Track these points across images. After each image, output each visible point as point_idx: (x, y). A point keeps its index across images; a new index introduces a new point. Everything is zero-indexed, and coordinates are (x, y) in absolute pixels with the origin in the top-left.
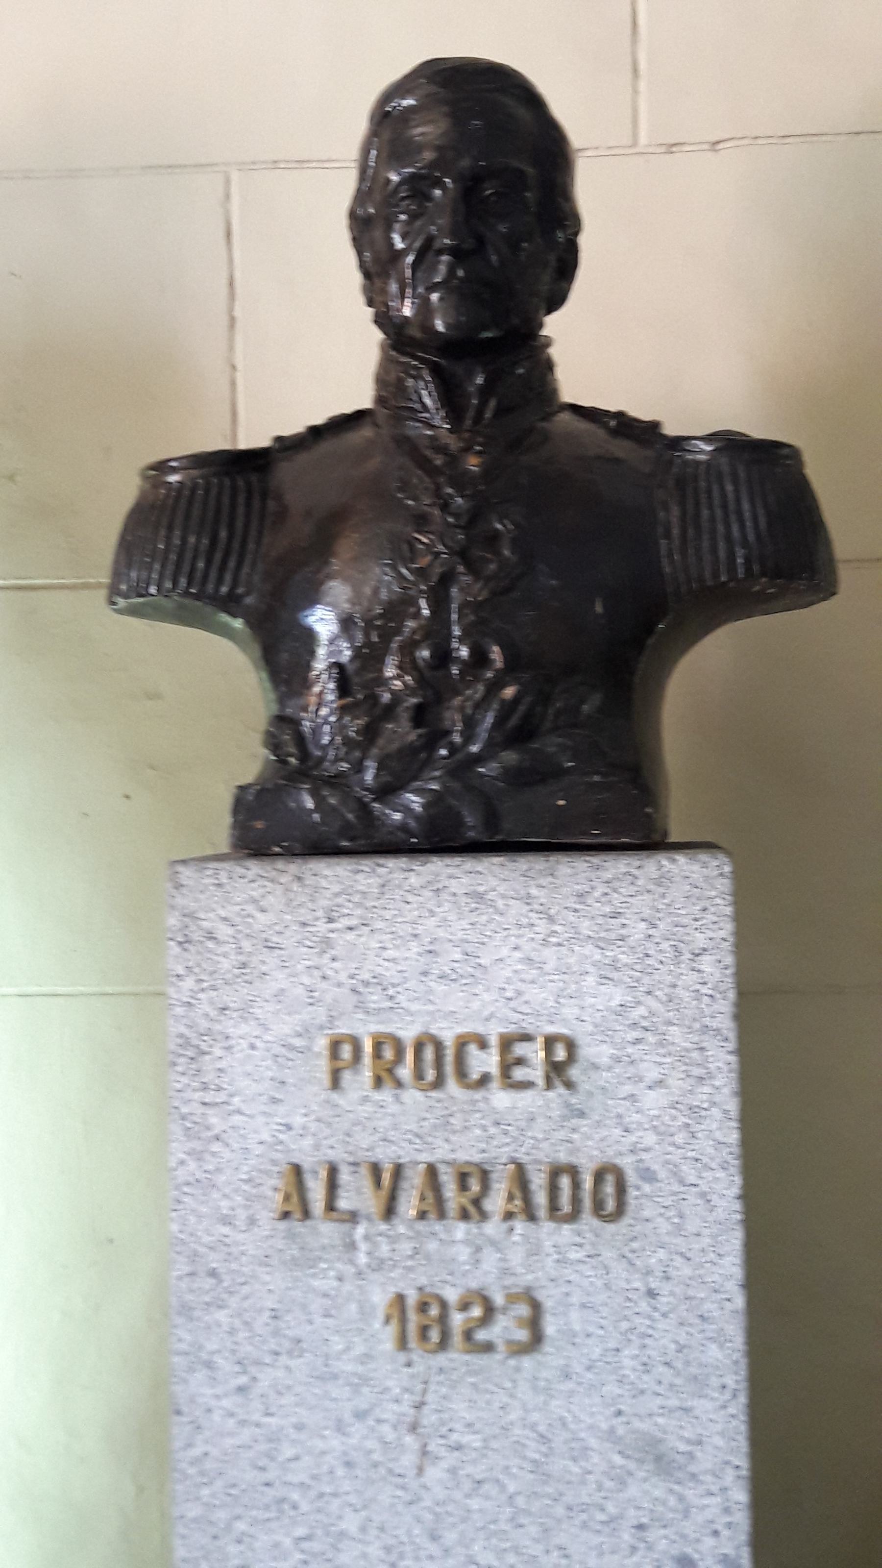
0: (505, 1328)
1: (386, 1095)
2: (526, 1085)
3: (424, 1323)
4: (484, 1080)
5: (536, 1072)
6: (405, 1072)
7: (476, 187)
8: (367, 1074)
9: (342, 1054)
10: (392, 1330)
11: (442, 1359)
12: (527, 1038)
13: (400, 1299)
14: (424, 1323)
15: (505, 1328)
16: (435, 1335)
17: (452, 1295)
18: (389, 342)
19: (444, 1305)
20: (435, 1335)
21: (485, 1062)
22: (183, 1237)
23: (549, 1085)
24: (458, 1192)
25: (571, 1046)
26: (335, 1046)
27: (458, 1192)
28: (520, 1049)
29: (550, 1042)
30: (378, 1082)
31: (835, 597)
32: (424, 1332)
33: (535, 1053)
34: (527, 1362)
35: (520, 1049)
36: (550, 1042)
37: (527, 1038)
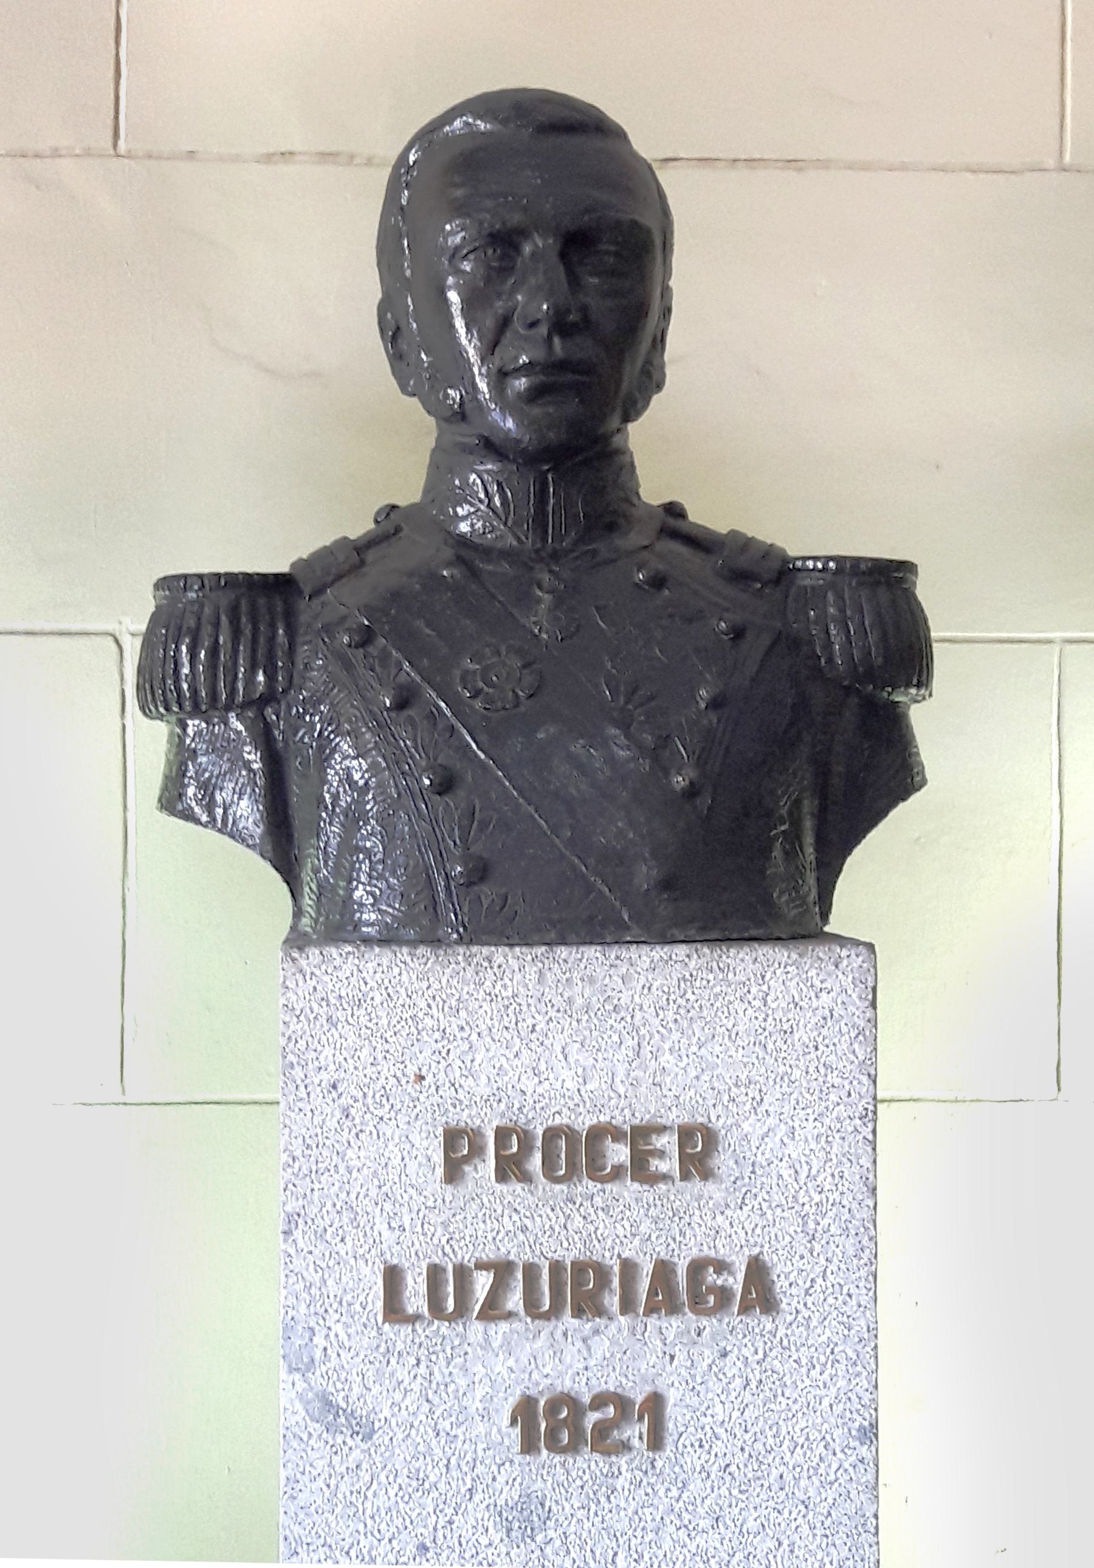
1: (282, 1237)
2: (665, 1177)
3: (551, 1424)
4: (617, 1173)
5: (669, 1165)
6: (536, 1162)
7: (544, 241)
8: (489, 1164)
9: (458, 1149)
12: (662, 1129)
14: (551, 1424)
16: (565, 1437)
18: (915, 750)
20: (565, 1437)
21: (619, 1153)
23: (685, 1176)
24: (579, 1289)
25: (710, 1137)
27: (579, 1289)
29: (686, 1134)
30: (502, 1176)
33: (668, 1142)
36: (686, 1134)
37: (662, 1129)
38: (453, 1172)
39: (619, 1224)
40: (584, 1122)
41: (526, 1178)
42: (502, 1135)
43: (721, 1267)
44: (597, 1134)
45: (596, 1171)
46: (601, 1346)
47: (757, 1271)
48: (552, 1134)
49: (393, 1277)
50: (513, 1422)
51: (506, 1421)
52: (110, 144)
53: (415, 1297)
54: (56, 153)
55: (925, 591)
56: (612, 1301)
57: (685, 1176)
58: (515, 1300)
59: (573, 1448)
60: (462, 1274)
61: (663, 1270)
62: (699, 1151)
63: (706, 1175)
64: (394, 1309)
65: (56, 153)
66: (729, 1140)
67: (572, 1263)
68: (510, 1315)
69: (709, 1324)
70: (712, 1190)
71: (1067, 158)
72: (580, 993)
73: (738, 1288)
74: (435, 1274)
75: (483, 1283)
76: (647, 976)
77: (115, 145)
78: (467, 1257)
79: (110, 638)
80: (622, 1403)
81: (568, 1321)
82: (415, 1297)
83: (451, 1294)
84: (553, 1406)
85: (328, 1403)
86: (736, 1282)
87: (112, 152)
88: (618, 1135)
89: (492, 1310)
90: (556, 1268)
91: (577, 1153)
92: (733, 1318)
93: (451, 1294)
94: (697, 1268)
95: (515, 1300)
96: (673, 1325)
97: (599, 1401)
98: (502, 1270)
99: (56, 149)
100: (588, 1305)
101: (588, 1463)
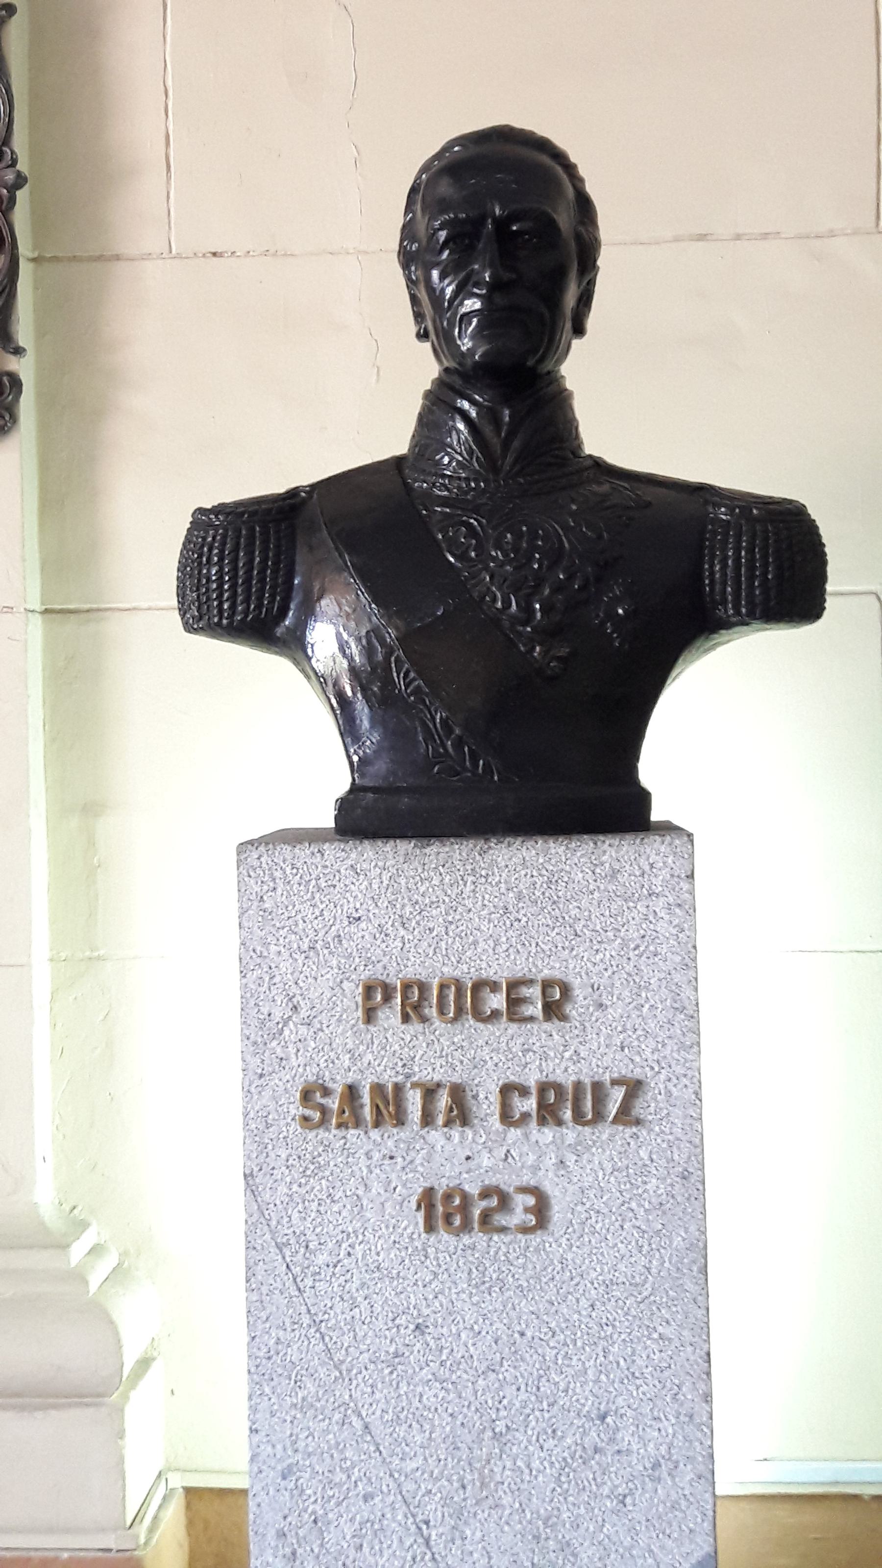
0: (518, 1216)
1: (416, 1027)
2: (531, 1019)
3: (443, 1210)
5: (536, 1009)
7: (506, 235)
9: (375, 995)
10: (420, 1217)
11: (466, 1240)
12: (530, 982)
13: (429, 1193)
14: (443, 1210)
15: (518, 1216)
16: (457, 1221)
17: (473, 1190)
19: (465, 1196)
20: (457, 1221)
21: (497, 1001)
22: (332, 1503)
25: (566, 990)
26: (369, 991)
28: (526, 992)
29: (547, 985)
30: (406, 1018)
31: (90, 1228)
32: (448, 1219)
33: (534, 992)
34: (535, 1239)
35: (526, 992)
37: (530, 982)
38: (370, 1016)
44: (478, 986)
50: (419, 1207)
51: (414, 1205)
52: (873, 224)
54: (832, 234)
59: (466, 1226)
61: (352, 1092)
63: (564, 1018)
65: (832, 234)
71: (174, 251)
73: (335, 1106)
76: (521, 864)
77: (877, 225)
79: (874, 596)
84: (448, 1197)
87: (874, 230)
88: (494, 987)
91: (465, 1000)
99: (832, 231)
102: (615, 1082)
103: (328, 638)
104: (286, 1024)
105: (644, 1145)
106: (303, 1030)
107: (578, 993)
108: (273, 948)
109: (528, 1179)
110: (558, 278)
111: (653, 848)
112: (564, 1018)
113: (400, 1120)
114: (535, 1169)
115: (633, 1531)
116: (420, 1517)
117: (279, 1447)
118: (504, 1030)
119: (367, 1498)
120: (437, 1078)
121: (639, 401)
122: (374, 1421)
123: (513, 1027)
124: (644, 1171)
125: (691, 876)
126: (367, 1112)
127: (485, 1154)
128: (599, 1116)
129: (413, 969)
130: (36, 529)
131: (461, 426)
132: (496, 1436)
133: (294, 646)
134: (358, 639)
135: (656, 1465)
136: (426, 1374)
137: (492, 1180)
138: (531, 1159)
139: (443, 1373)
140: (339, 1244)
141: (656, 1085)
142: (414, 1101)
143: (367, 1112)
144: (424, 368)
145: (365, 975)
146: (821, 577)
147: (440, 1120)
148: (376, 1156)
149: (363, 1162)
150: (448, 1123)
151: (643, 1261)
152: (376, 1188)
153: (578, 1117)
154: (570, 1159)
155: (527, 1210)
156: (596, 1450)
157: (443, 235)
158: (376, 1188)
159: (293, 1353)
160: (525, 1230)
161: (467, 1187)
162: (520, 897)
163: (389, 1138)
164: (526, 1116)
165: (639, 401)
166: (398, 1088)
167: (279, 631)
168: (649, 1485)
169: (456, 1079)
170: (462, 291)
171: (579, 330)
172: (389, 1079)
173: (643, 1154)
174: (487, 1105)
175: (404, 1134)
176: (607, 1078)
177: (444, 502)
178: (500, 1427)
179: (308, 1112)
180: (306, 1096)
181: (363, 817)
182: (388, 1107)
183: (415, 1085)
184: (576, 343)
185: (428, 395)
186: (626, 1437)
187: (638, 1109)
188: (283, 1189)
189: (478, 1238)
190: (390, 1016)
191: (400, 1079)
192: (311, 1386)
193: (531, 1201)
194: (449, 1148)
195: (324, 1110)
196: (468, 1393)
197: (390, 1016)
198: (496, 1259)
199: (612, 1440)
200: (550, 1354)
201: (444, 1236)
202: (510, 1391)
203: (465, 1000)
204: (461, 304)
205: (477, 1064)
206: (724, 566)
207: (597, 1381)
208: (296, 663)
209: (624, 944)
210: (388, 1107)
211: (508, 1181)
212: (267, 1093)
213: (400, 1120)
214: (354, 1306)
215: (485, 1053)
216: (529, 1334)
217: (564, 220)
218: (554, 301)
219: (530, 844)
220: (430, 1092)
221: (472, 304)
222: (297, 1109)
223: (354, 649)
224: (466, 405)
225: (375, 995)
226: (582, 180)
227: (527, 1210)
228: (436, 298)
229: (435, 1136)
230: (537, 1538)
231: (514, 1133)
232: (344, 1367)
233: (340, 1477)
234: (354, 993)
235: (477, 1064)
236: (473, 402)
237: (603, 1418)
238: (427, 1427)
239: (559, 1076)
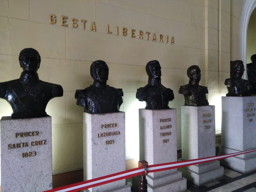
3: (25, 155)
4: (31, 135)
5: (114, 126)
6: (107, 127)
9: (17, 135)
21: (31, 134)
24: (109, 134)
25: (116, 124)
27: (109, 134)
28: (34, 133)
29: (115, 124)
30: (105, 127)
35: (34, 133)
36: (115, 124)
39: (112, 130)
40: (109, 124)
41: (106, 128)
42: (105, 125)
43: (117, 132)
44: (110, 124)
45: (29, 135)
46: (111, 137)
47: (119, 132)
48: (108, 125)
49: (99, 135)
53: (100, 136)
55: (123, 90)
56: (111, 135)
57: (37, 135)
58: (106, 135)
59: (27, 156)
60: (103, 134)
61: (114, 132)
62: (116, 125)
64: (99, 137)
66: (117, 124)
67: (17, 144)
68: (105, 136)
69: (116, 135)
70: (117, 127)
72: (109, 116)
74: (101, 134)
75: (104, 134)
78: (103, 133)
80: (112, 141)
81: (109, 136)
82: (100, 136)
83: (102, 135)
84: (25, 154)
85: (94, 143)
86: (118, 133)
88: (31, 133)
89: (104, 136)
90: (108, 133)
91: (27, 134)
92: (118, 135)
93: (102, 135)
94: (116, 132)
95: (106, 135)
96: (114, 136)
97: (111, 141)
98: (105, 133)
100: (110, 135)
101: (110, 145)
102: (43, 140)
103: (10, 97)
104: (6, 139)
105: (46, 146)
106: (8, 139)
107: (40, 132)
108: (5, 131)
109: (34, 151)
110: (37, 63)
111: (48, 119)
112: (38, 135)
113: (20, 147)
114: (35, 150)
115: (44, 182)
116: (21, 186)
117: (5, 182)
118: (167, 122)
119: (15, 185)
120: (24, 142)
121: (45, 74)
122: (17, 178)
123: (33, 136)
124: (46, 148)
125: (51, 121)
126: (16, 147)
127: (29, 149)
128: (42, 144)
129: (22, 131)
130: (152, 152)
131: (26, 76)
132: (30, 176)
133: (6, 99)
134: (14, 98)
135: (47, 175)
136: (22, 171)
137: (30, 151)
138: (34, 149)
139: (24, 171)
140: (12, 160)
141: (47, 141)
142: (22, 145)
143: (16, 147)
144: (22, 70)
145: (16, 133)
146: (63, 91)
147: (24, 146)
148: (17, 151)
149: (15, 151)
150: (25, 146)
151: (46, 157)
152: (17, 154)
153: (40, 144)
154: (38, 148)
155: (34, 154)
156: (41, 175)
157: (24, 58)
158: (17, 154)
159: (7, 172)
160: (34, 156)
161: (27, 153)
162: (33, 124)
163: (19, 149)
164: (34, 145)
165: (45, 74)
166: (20, 144)
167: (4, 97)
168: (46, 177)
169: (26, 142)
170: (27, 64)
171: (39, 68)
172: (19, 143)
173: (46, 147)
174: (30, 144)
175: (20, 148)
176: (42, 140)
177: (24, 84)
178: (31, 175)
179: (9, 147)
180: (9, 146)
181: (15, 116)
182: (18, 146)
183: (22, 143)
184: (38, 69)
185: (22, 73)
186: (44, 173)
187: (46, 143)
188: (6, 156)
189: (29, 157)
190: (19, 137)
191: (20, 143)
192: (9, 175)
193: (34, 153)
194: (25, 149)
195: (11, 147)
196: (27, 172)
197: (19, 137)
198: (30, 159)
199: (42, 174)
200: (36, 167)
201: (25, 158)
202: (32, 171)
203: (27, 134)
204: (26, 65)
205: (29, 140)
206: (54, 91)
207: (41, 169)
208: (6, 100)
209: (44, 127)
210: (18, 146)
211: (31, 151)
212: (4, 146)
213: (20, 147)
214: (14, 166)
215: (30, 139)
216: (34, 165)
217: (38, 58)
218: (37, 65)
219: (35, 119)
220: (23, 144)
221: (28, 65)
222: (8, 147)
223: (14, 100)
224: (27, 75)
225: (17, 135)
226: (39, 54)
227: (34, 154)
228: (24, 64)
229: (24, 148)
230: (34, 185)
231: (33, 147)
232: (13, 173)
233: (12, 184)
234: (14, 135)
235: (29, 140)
236: (27, 74)
237: (41, 172)
238: (22, 177)
239: (37, 140)
